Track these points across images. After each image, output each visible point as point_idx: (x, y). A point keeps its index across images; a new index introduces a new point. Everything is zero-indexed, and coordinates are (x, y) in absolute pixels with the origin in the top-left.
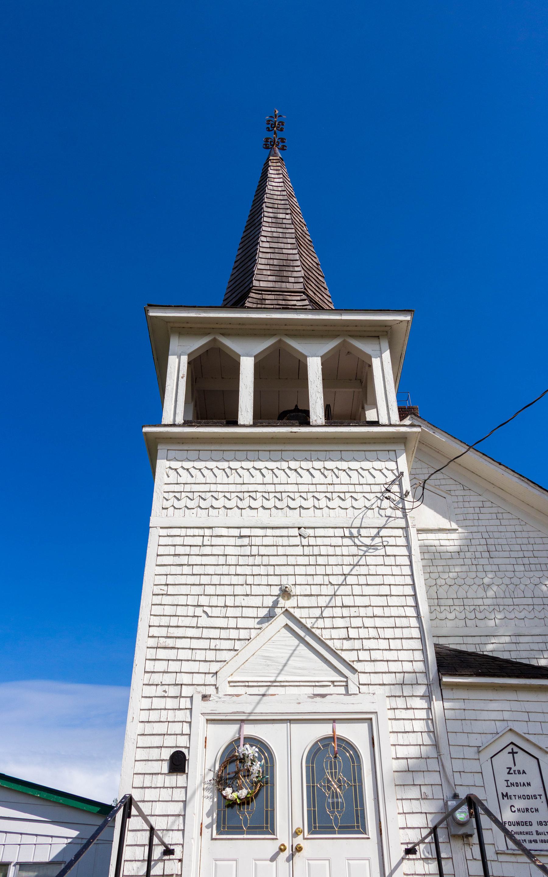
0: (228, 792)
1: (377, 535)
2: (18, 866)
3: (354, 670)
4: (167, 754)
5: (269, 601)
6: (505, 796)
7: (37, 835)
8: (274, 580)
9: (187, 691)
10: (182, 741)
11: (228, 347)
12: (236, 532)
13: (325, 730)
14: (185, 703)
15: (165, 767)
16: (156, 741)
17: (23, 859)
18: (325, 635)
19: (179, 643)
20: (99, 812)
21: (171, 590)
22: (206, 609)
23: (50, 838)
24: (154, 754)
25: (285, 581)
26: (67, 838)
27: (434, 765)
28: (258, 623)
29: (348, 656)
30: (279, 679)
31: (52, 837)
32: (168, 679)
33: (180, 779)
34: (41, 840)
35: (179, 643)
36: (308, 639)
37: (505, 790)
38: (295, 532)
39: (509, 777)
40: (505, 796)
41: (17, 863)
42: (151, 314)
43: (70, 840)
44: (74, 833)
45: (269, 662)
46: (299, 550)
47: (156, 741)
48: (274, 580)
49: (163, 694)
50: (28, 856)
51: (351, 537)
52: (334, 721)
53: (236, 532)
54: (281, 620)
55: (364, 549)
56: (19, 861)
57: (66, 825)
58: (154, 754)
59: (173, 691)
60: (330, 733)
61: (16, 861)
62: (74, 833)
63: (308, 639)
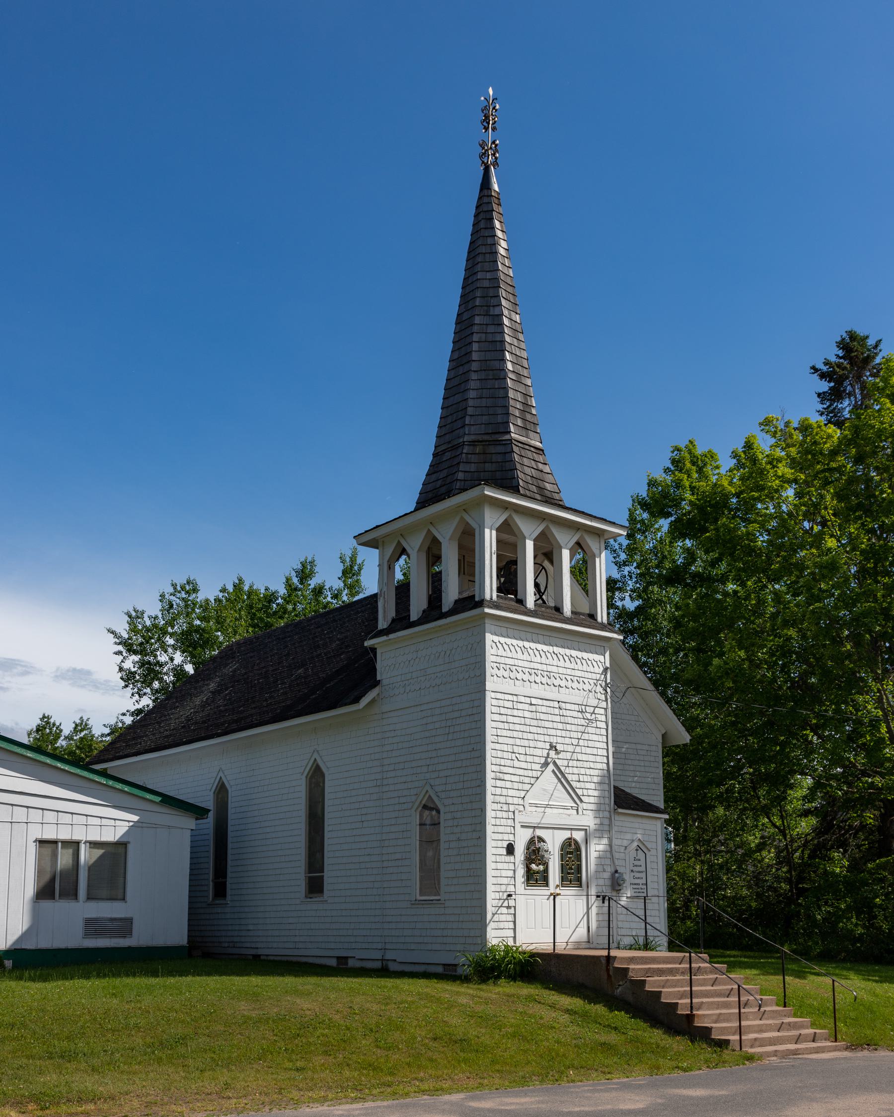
0: (534, 866)
1: (593, 713)
2: (88, 844)
3: (581, 801)
4: (505, 844)
5: (545, 753)
6: (632, 871)
7: (101, 818)
8: (547, 738)
9: (512, 808)
10: (511, 837)
11: (517, 525)
12: (528, 700)
13: (566, 834)
14: (511, 815)
15: (504, 852)
16: (500, 837)
17: (96, 838)
18: (569, 777)
19: (507, 777)
20: (160, 801)
21: (501, 740)
22: (517, 755)
23: (113, 821)
24: (500, 844)
25: (554, 740)
26: (129, 821)
27: (609, 855)
28: (541, 767)
29: (579, 792)
30: (550, 803)
31: (115, 819)
32: (502, 799)
33: (512, 858)
34: (105, 822)
35: (507, 777)
36: (563, 780)
37: (632, 868)
38: (556, 704)
39: (634, 862)
40: (632, 871)
41: (86, 842)
42: (486, 493)
43: (131, 824)
44: (135, 818)
45: (545, 793)
46: (557, 719)
47: (500, 837)
48: (547, 738)
49: (500, 809)
50: (95, 836)
51: (582, 712)
52: (571, 829)
53: (528, 700)
54: (551, 767)
55: (587, 721)
56: (88, 839)
57: (127, 810)
58: (500, 844)
59: (505, 807)
60: (569, 836)
61: (84, 840)
62: (135, 818)
63: (563, 780)
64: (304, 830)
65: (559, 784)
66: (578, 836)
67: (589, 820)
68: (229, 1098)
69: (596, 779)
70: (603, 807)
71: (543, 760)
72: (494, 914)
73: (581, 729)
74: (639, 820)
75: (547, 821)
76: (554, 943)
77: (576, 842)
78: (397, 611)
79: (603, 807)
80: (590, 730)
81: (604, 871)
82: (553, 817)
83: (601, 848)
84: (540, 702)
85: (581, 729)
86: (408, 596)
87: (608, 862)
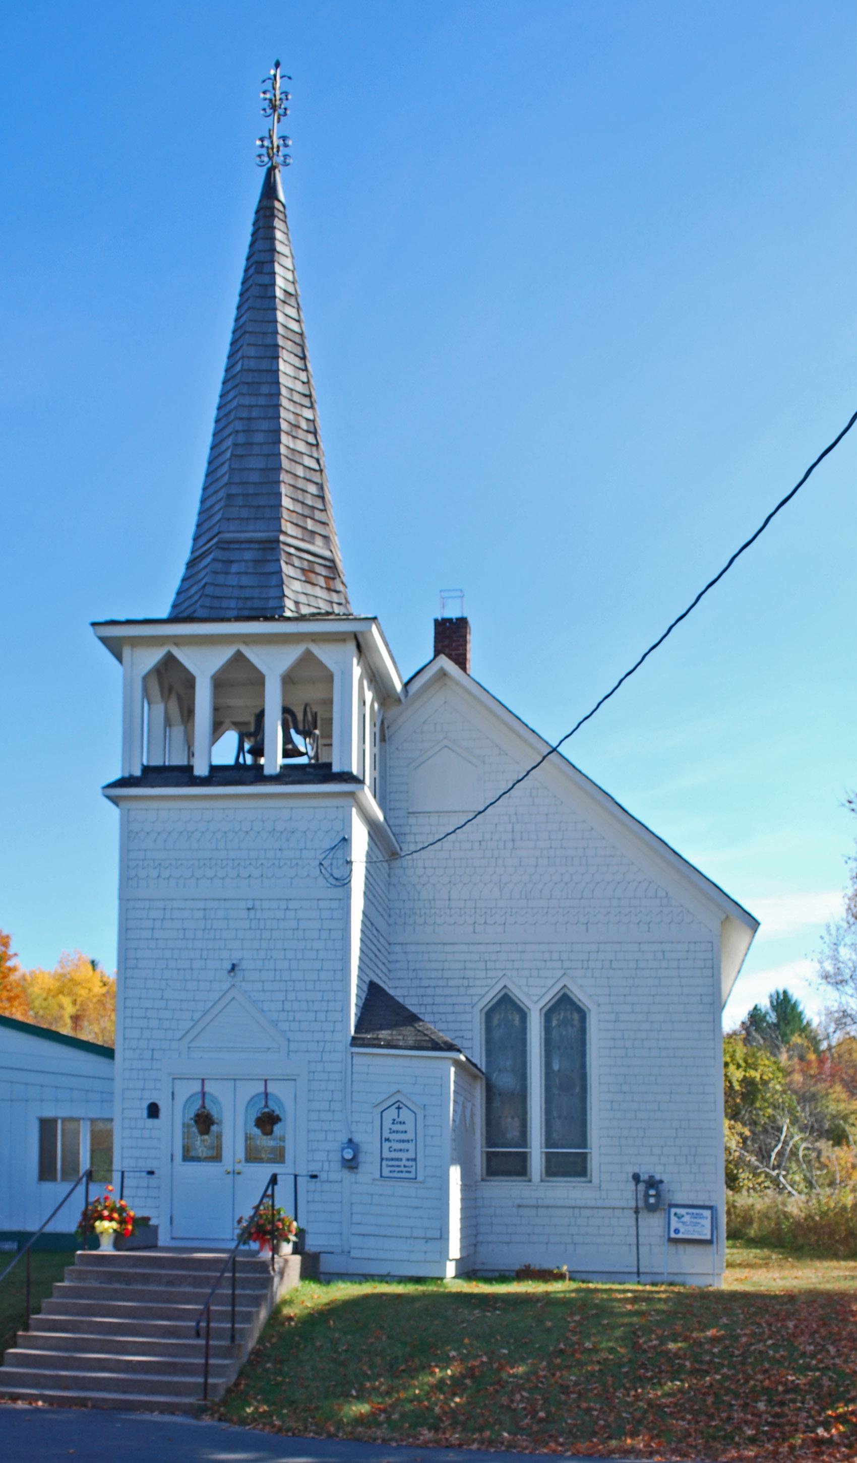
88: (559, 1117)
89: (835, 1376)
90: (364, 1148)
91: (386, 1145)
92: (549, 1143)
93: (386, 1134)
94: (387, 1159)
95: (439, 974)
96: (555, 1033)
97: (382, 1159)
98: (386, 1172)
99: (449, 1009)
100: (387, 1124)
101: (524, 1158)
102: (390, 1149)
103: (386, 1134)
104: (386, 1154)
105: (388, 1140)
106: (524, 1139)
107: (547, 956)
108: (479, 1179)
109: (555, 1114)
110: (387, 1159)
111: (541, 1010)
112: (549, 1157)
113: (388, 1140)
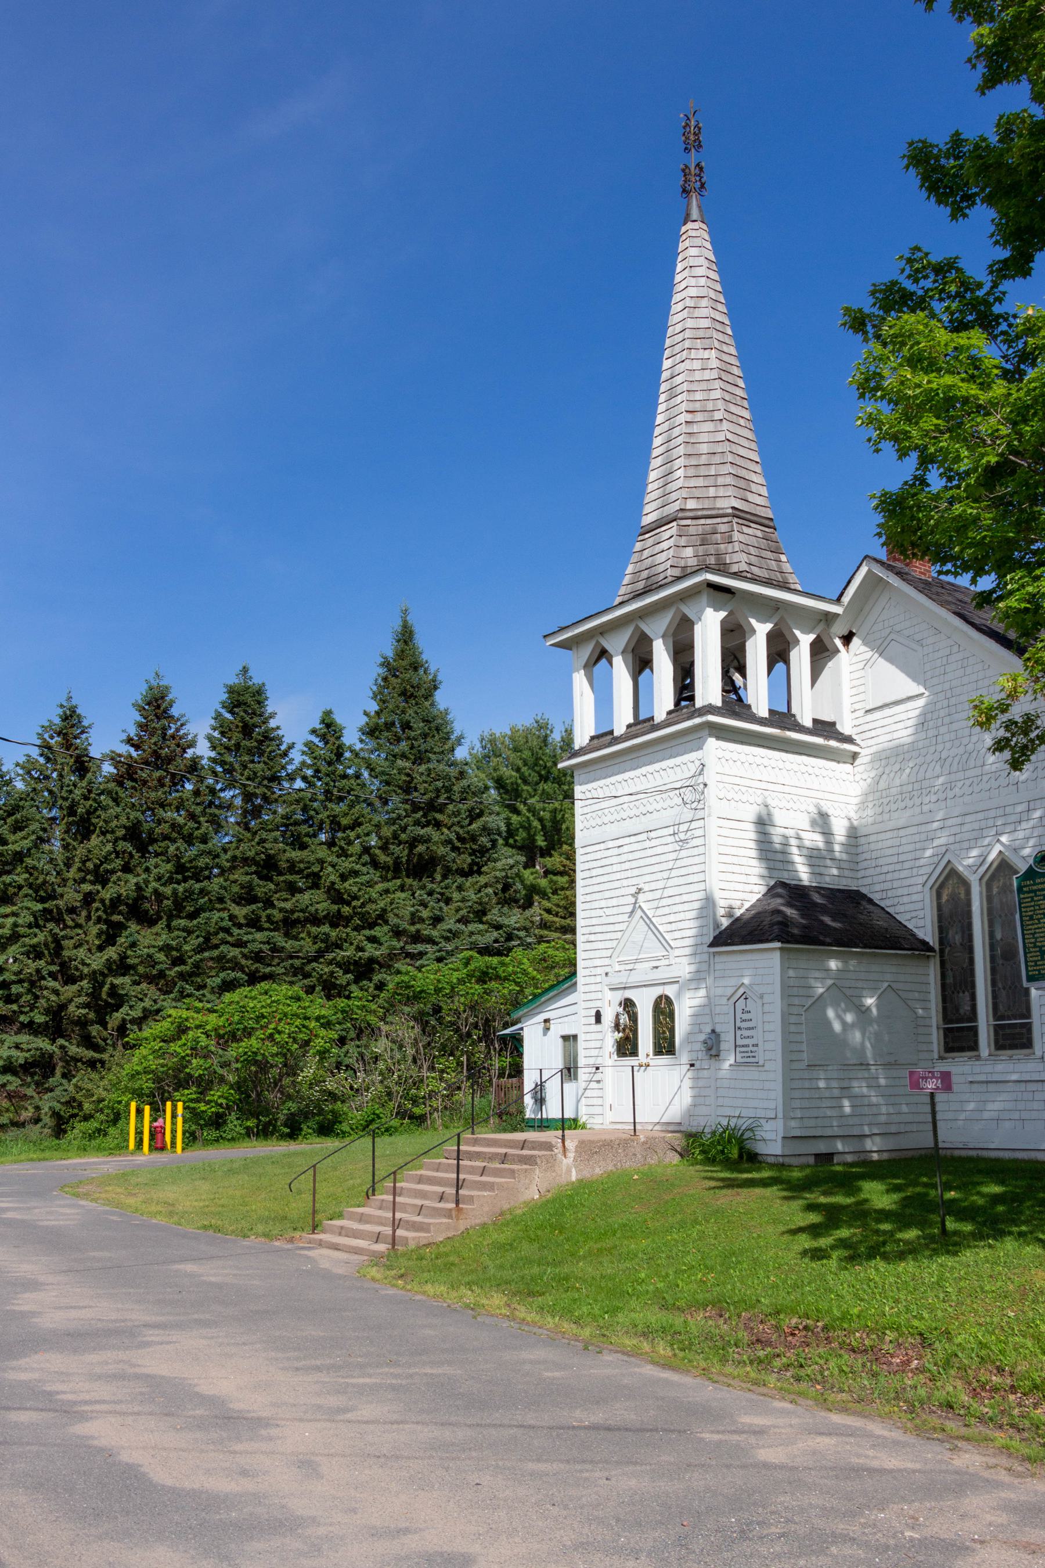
4: (593, 1012)
13: (658, 991)
64: (928, 900)
65: (650, 932)
66: (670, 991)
67: (683, 967)
68: (862, 1300)
69: (693, 914)
70: (700, 949)
71: (629, 909)
72: (585, 1089)
73: (673, 856)
74: (748, 956)
75: (634, 978)
76: (635, 1123)
77: (667, 998)
78: (742, 648)
79: (700, 949)
80: (683, 853)
81: (701, 1032)
82: (643, 972)
83: (697, 1002)
84: (627, 840)
85: (673, 856)
86: (612, 708)
87: (707, 1019)
88: (1004, 988)
89: (1024, 1228)
90: (723, 1037)
91: (739, 1033)
92: (997, 1014)
93: (738, 1024)
94: (740, 1046)
95: (895, 859)
96: (996, 901)
97: (736, 1046)
98: (739, 1059)
99: (905, 891)
100: (739, 1015)
101: (974, 1030)
102: (743, 1037)
103: (738, 1024)
104: (739, 1042)
105: (739, 1028)
106: (973, 1016)
107: (983, 824)
108: (936, 1056)
109: (1000, 985)
110: (740, 1046)
111: (980, 879)
112: (997, 1029)
113: (739, 1028)
